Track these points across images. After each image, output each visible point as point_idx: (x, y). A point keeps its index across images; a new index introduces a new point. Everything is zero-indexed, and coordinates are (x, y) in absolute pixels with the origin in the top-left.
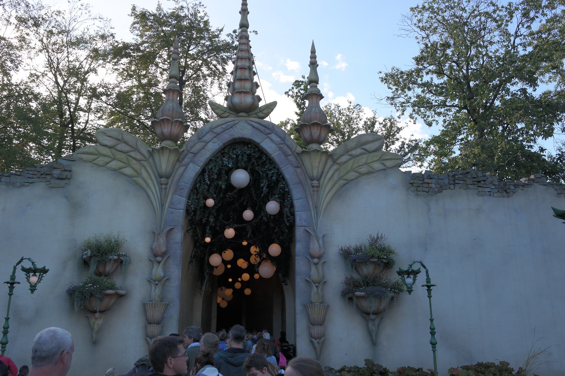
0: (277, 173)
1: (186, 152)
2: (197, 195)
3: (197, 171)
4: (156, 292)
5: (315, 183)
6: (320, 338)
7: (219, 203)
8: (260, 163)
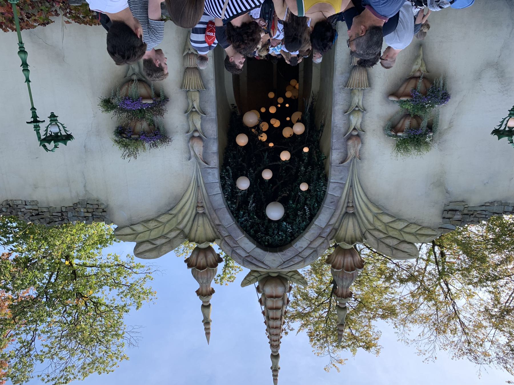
0: (238, 219)
1: (329, 238)
2: (317, 195)
3: (317, 220)
4: (358, 99)
5: (200, 211)
6: (188, 54)
7: (296, 186)
8: (256, 227)
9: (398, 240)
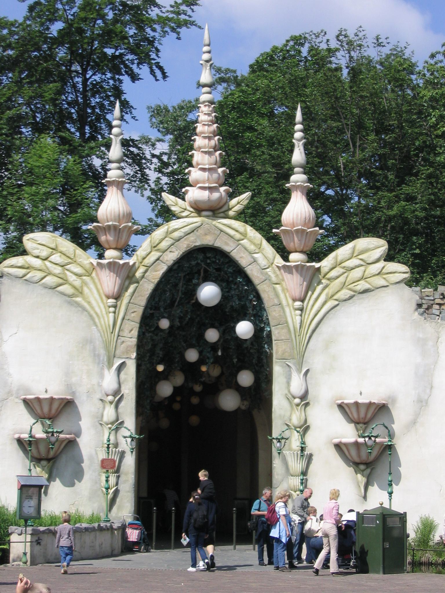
9: (53, 261)
